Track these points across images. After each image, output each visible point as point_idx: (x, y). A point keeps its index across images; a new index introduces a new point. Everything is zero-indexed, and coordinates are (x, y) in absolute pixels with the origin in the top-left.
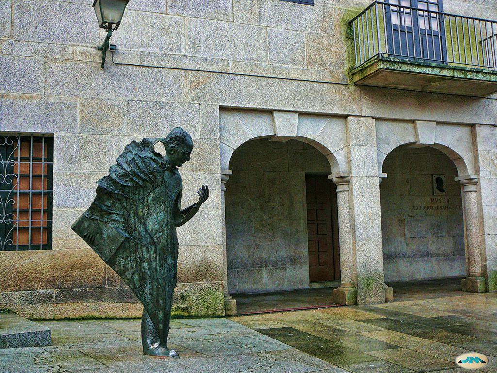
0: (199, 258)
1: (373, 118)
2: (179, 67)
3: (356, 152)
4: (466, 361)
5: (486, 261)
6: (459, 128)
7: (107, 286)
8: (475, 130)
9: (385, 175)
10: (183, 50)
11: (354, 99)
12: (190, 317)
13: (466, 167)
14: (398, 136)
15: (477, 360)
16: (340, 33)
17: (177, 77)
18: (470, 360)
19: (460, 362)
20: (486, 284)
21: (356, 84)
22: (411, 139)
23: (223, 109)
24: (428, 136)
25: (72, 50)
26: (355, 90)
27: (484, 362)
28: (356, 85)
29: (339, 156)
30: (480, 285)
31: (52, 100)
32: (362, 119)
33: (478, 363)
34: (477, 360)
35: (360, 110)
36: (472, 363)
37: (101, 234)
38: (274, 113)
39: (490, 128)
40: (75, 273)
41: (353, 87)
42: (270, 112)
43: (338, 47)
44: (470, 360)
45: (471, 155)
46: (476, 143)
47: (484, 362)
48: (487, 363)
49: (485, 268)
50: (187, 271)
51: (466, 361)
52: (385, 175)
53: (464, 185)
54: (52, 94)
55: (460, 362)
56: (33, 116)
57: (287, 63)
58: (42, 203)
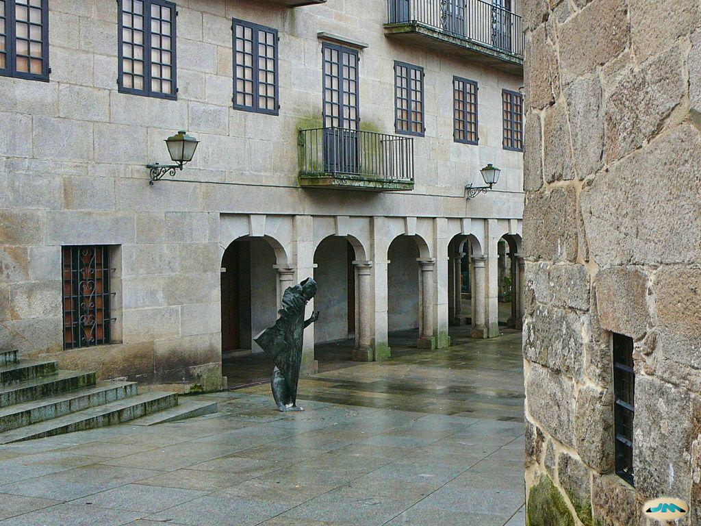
0: (207, 344)
1: (311, 216)
2: (196, 180)
3: (300, 246)
4: (657, 509)
5: (374, 335)
6: (361, 219)
7: (155, 372)
8: (373, 221)
9: (316, 266)
10: (198, 164)
11: (300, 201)
12: (203, 393)
13: (479, 243)
14: (325, 230)
15: (673, 507)
16: (293, 140)
17: (195, 189)
18: (663, 508)
19: (649, 511)
20: (374, 355)
21: (303, 187)
22: (332, 232)
23: (222, 215)
24: (343, 232)
25: (130, 169)
26: (302, 192)
27: (682, 511)
28: (303, 188)
29: (288, 250)
30: (370, 355)
31: (120, 215)
32: (305, 217)
33: (674, 512)
34: (673, 507)
35: (304, 211)
36: (666, 512)
37: (273, 342)
38: (251, 216)
39: (383, 219)
40: (137, 362)
41: (300, 189)
42: (248, 215)
43: (292, 153)
44: (663, 508)
45: (368, 243)
46: (373, 233)
47: (682, 511)
48: (687, 511)
49: (373, 341)
50: (201, 355)
51: (657, 509)
52: (316, 266)
53: (280, 274)
54: (119, 210)
55: (649, 511)
56: (109, 230)
57: (261, 171)
58: (99, 303)
